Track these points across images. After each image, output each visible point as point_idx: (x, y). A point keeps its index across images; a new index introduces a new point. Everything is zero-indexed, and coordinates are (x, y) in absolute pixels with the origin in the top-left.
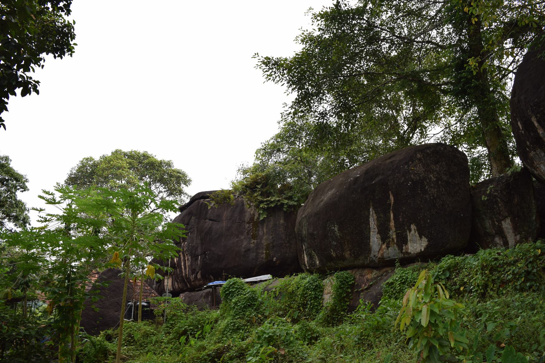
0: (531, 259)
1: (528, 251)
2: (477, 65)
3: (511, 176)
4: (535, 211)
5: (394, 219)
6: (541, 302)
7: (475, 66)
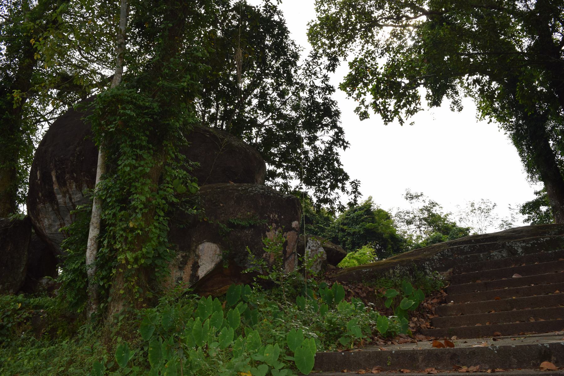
0: (9, 313)
1: (8, 303)
2: (21, 99)
3: (11, 223)
4: (24, 263)
5: (505, 350)
6: (9, 359)
7: (18, 99)
